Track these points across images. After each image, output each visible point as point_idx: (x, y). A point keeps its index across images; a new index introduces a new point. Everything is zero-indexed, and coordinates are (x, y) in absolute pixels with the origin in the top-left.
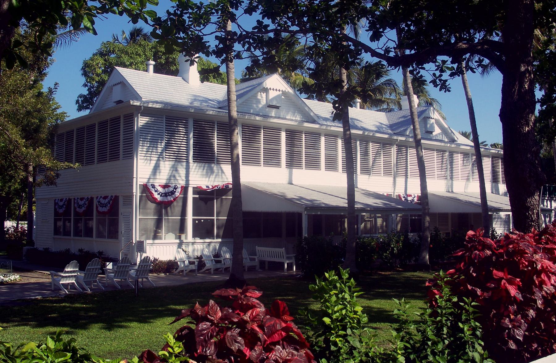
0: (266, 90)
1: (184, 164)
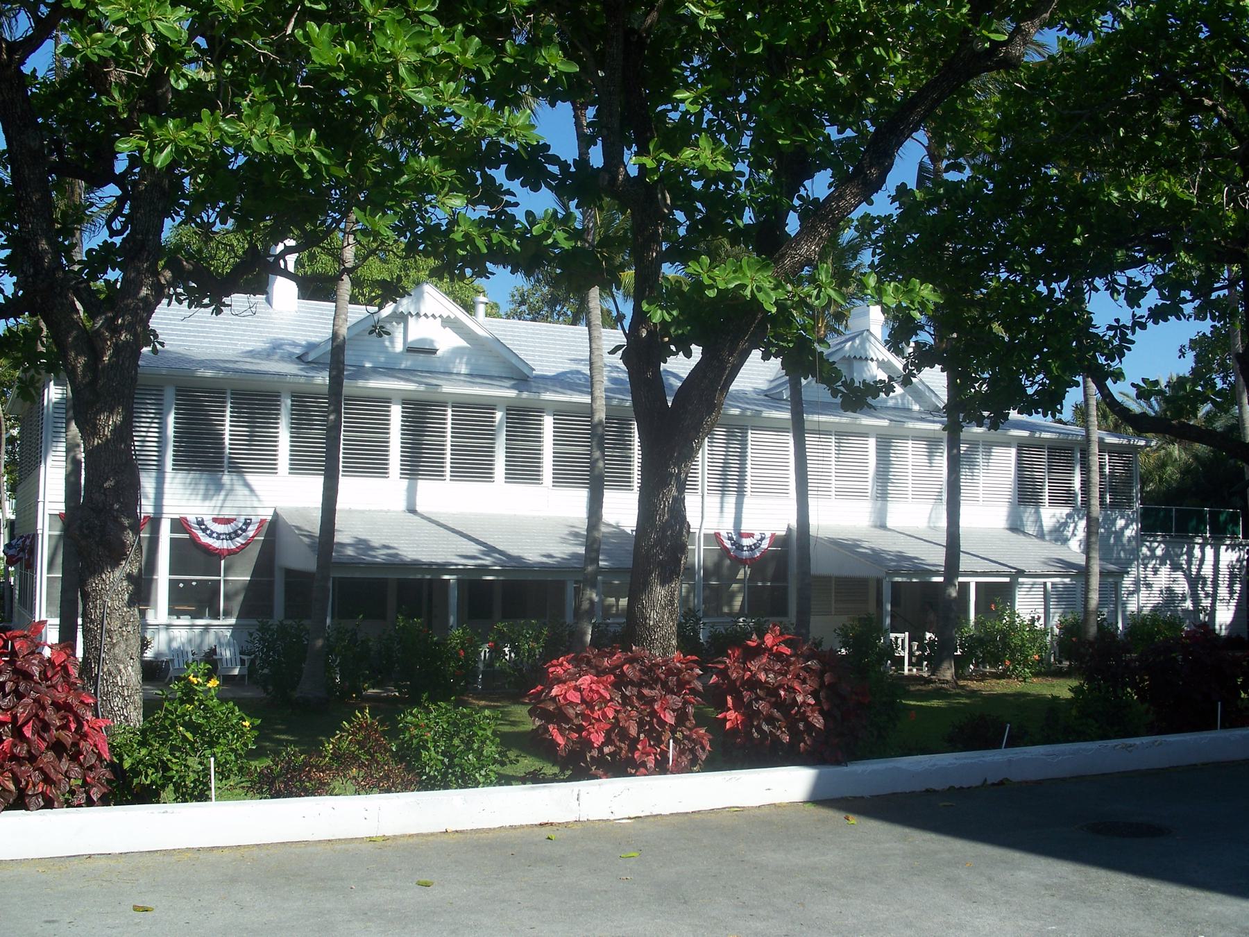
1: (154, 474)
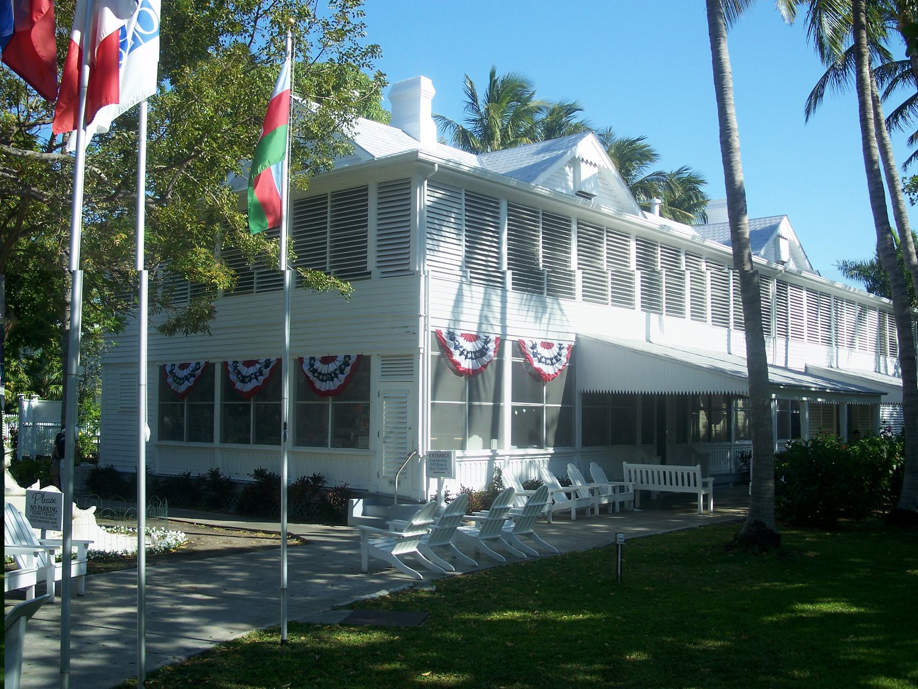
0: (575, 162)
